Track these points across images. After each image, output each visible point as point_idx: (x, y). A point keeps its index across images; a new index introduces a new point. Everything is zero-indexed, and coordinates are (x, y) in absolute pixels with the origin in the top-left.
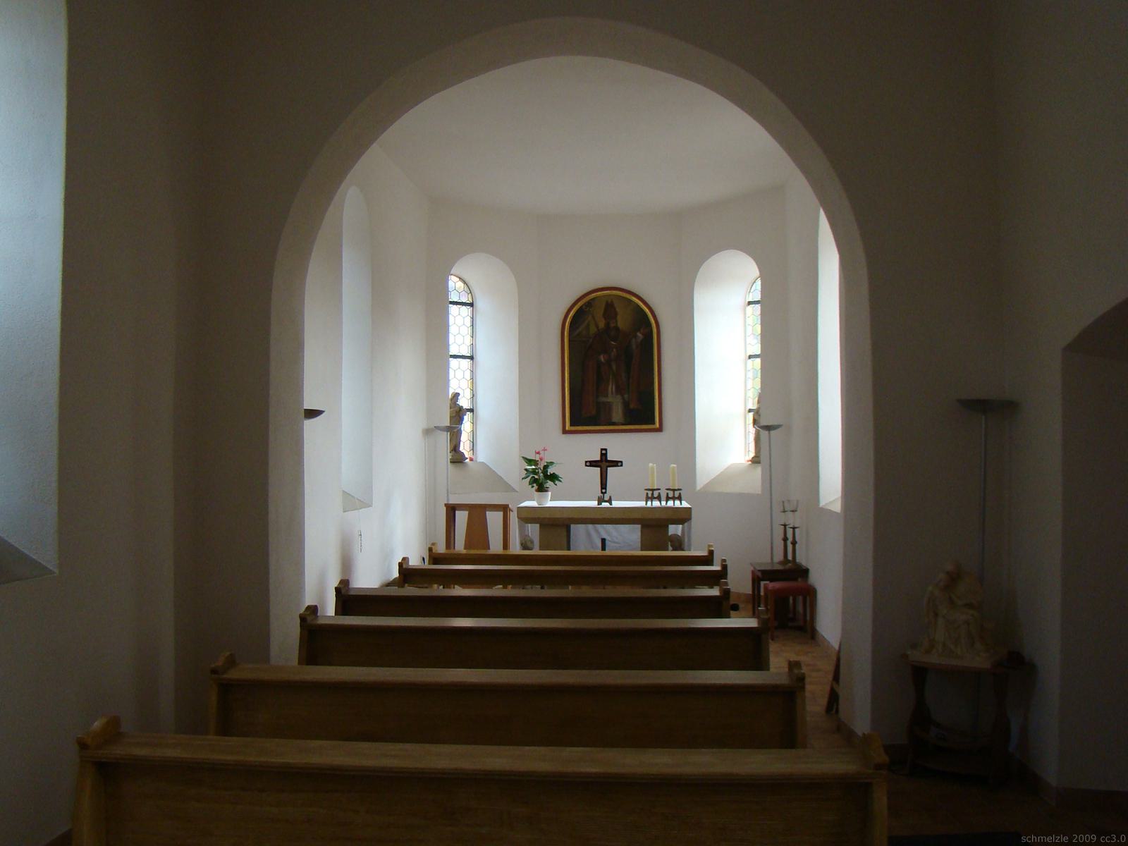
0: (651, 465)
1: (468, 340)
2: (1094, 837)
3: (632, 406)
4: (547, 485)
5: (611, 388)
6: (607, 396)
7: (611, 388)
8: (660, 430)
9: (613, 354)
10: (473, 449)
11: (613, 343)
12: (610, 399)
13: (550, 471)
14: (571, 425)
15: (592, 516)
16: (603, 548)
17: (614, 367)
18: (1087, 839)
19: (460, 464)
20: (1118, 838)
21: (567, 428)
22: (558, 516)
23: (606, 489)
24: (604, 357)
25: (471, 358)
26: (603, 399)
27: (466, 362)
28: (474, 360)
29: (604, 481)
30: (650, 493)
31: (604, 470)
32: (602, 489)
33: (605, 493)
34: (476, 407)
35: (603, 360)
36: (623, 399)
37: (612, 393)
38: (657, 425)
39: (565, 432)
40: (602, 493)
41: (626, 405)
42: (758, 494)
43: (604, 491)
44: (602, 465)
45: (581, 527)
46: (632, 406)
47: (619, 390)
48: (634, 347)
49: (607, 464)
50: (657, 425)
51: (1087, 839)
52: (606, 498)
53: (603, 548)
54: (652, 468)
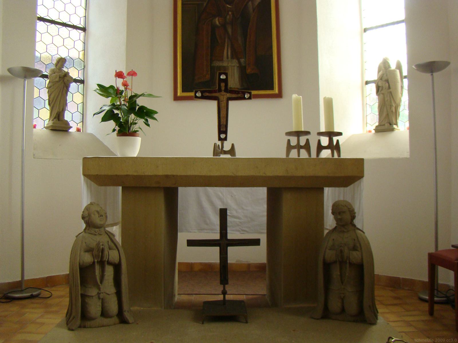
0: (295, 96)
1: (81, 12)
2: (444, 340)
3: (249, 71)
4: (135, 128)
5: (227, 52)
6: (222, 60)
7: (227, 52)
8: (279, 95)
9: (228, 17)
10: (83, 122)
11: (228, 6)
12: (225, 64)
13: (140, 102)
14: (184, 90)
15: (205, 172)
16: (256, 242)
17: (230, 30)
18: (441, 340)
19: (66, 132)
20: (454, 340)
21: (179, 94)
22: (149, 171)
23: (226, 132)
24: (218, 20)
25: (84, 29)
26: (217, 64)
27: (76, 34)
28: (86, 31)
29: (223, 121)
30: (294, 141)
31: (223, 104)
32: (220, 132)
33: (225, 139)
34: (87, 80)
35: (217, 23)
36: (239, 63)
37: (228, 58)
38: (276, 91)
39: (176, 98)
40: (220, 139)
41: (242, 69)
42: (406, 158)
43: (223, 136)
44: (221, 98)
45: (191, 190)
46: (249, 71)
47: (235, 55)
48: (251, 10)
49: (229, 95)
50: (276, 91)
51: (441, 340)
52: (227, 146)
53: (256, 242)
54: (298, 101)
